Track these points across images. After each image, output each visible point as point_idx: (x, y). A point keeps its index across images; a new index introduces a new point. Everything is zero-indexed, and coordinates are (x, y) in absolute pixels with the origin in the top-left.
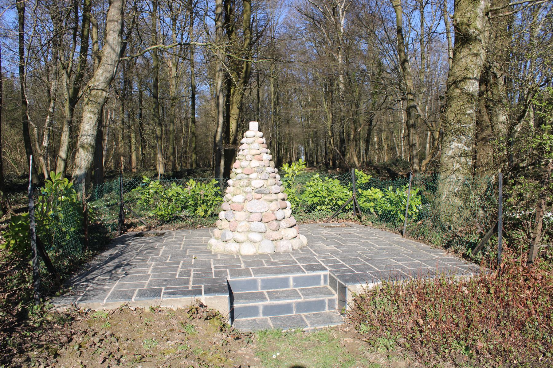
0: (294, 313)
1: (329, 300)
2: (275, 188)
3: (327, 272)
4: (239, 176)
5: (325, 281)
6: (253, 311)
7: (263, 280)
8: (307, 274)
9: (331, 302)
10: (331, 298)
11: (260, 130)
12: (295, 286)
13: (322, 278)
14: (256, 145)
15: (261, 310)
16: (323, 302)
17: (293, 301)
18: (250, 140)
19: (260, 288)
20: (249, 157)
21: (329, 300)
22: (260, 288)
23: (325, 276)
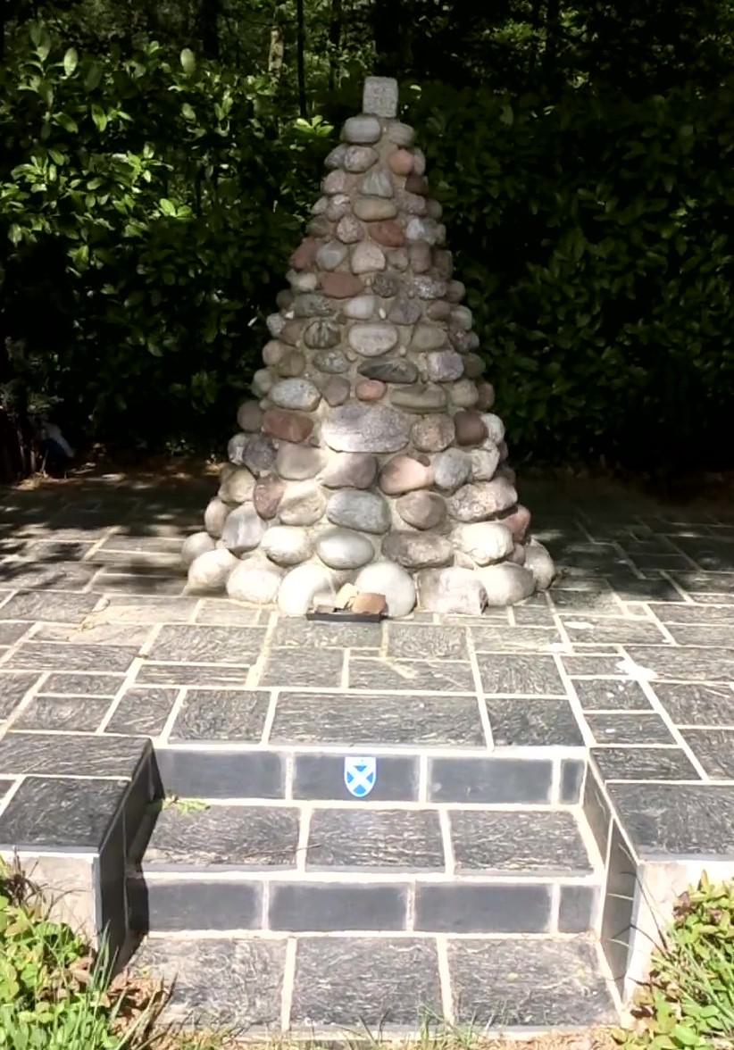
0: (409, 930)
1: (567, 892)
2: (434, 364)
3: (580, 754)
4: (304, 302)
5: (569, 791)
6: (232, 905)
7: (281, 797)
8: (494, 751)
9: (576, 899)
10: (576, 881)
11: (403, 117)
12: (437, 797)
13: (557, 776)
14: (378, 183)
15: (266, 901)
16: (544, 768)
17: (410, 879)
18: (358, 157)
19: (288, 791)
20: (347, 229)
21: (567, 892)
22: (288, 791)
23: (571, 769)
